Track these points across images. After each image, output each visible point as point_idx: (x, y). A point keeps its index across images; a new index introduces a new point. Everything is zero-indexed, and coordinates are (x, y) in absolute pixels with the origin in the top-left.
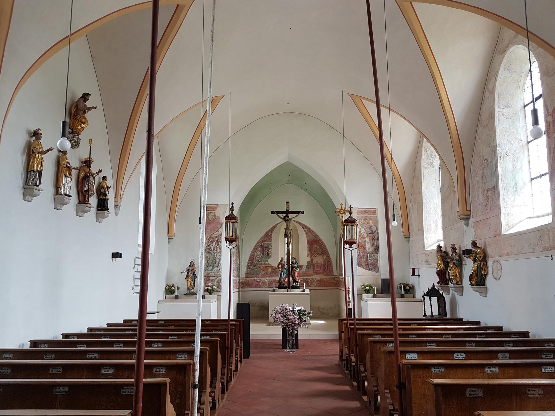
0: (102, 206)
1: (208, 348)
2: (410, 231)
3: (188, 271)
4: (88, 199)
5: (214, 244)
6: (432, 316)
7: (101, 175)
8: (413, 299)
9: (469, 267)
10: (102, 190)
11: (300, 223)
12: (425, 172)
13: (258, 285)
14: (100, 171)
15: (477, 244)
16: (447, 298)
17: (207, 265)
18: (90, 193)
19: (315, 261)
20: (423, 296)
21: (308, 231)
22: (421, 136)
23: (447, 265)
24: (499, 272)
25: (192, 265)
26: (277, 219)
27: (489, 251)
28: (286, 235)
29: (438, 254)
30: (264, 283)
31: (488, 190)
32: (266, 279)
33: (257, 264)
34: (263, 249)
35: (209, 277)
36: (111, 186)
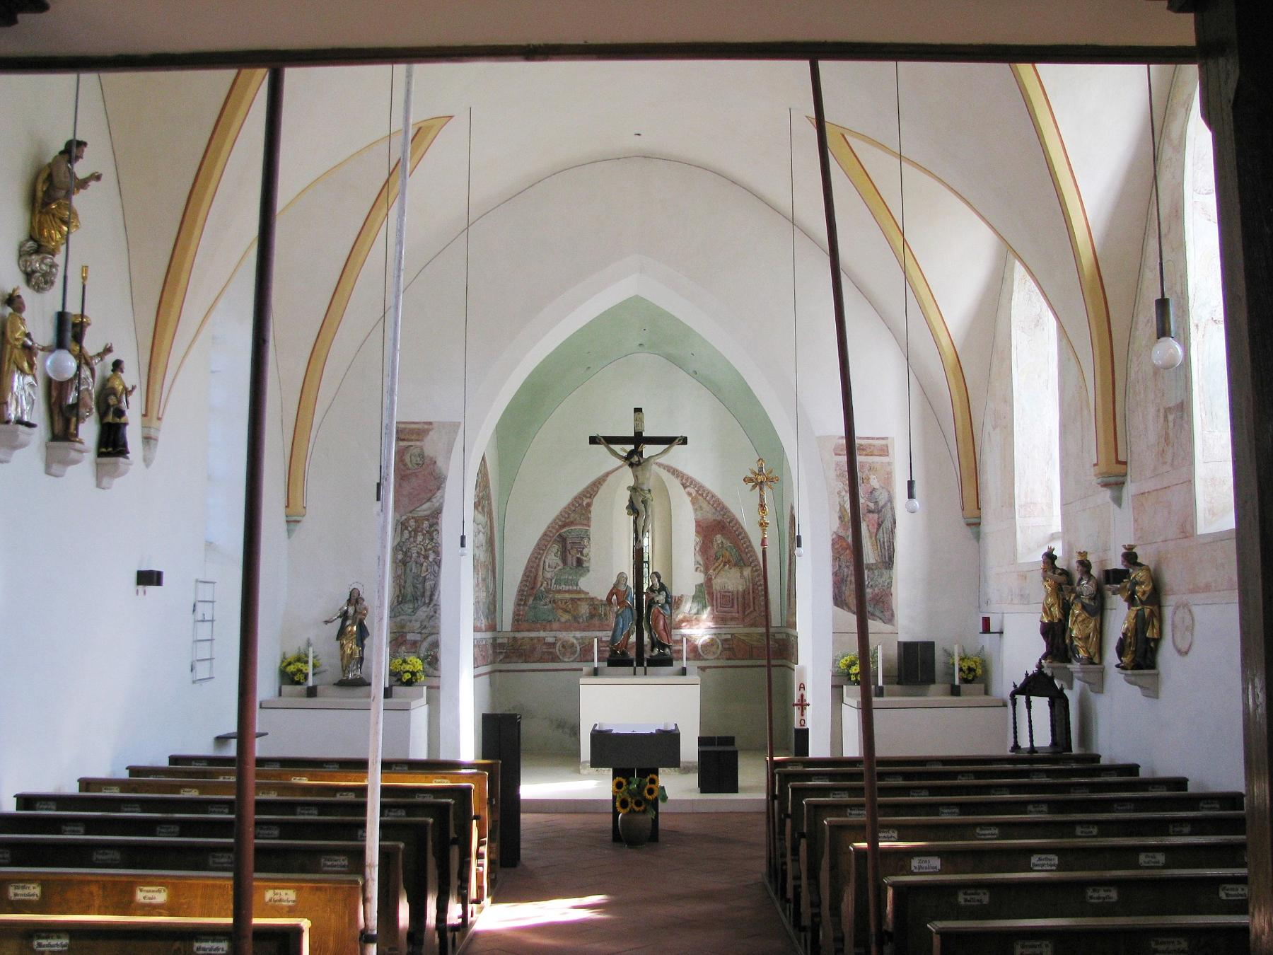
0: (112, 443)
1: (402, 845)
2: (982, 504)
3: (344, 616)
4: (77, 429)
5: (420, 538)
6: (1032, 749)
7: (110, 359)
8: (982, 699)
9: (1119, 617)
10: (112, 400)
11: (674, 472)
12: (1019, 340)
13: (550, 654)
14: (108, 350)
15: (1135, 556)
16: (1072, 696)
17: (400, 600)
18: (82, 411)
19: (718, 583)
20: (1013, 695)
21: (700, 494)
22: (1008, 251)
23: (1066, 609)
24: (1188, 634)
25: (355, 598)
26: (606, 460)
27: (1172, 577)
28: (633, 508)
29: (1045, 579)
30: (568, 647)
31: (1168, 410)
32: (572, 637)
33: (548, 591)
34: (564, 547)
35: (403, 635)
36: (134, 388)
